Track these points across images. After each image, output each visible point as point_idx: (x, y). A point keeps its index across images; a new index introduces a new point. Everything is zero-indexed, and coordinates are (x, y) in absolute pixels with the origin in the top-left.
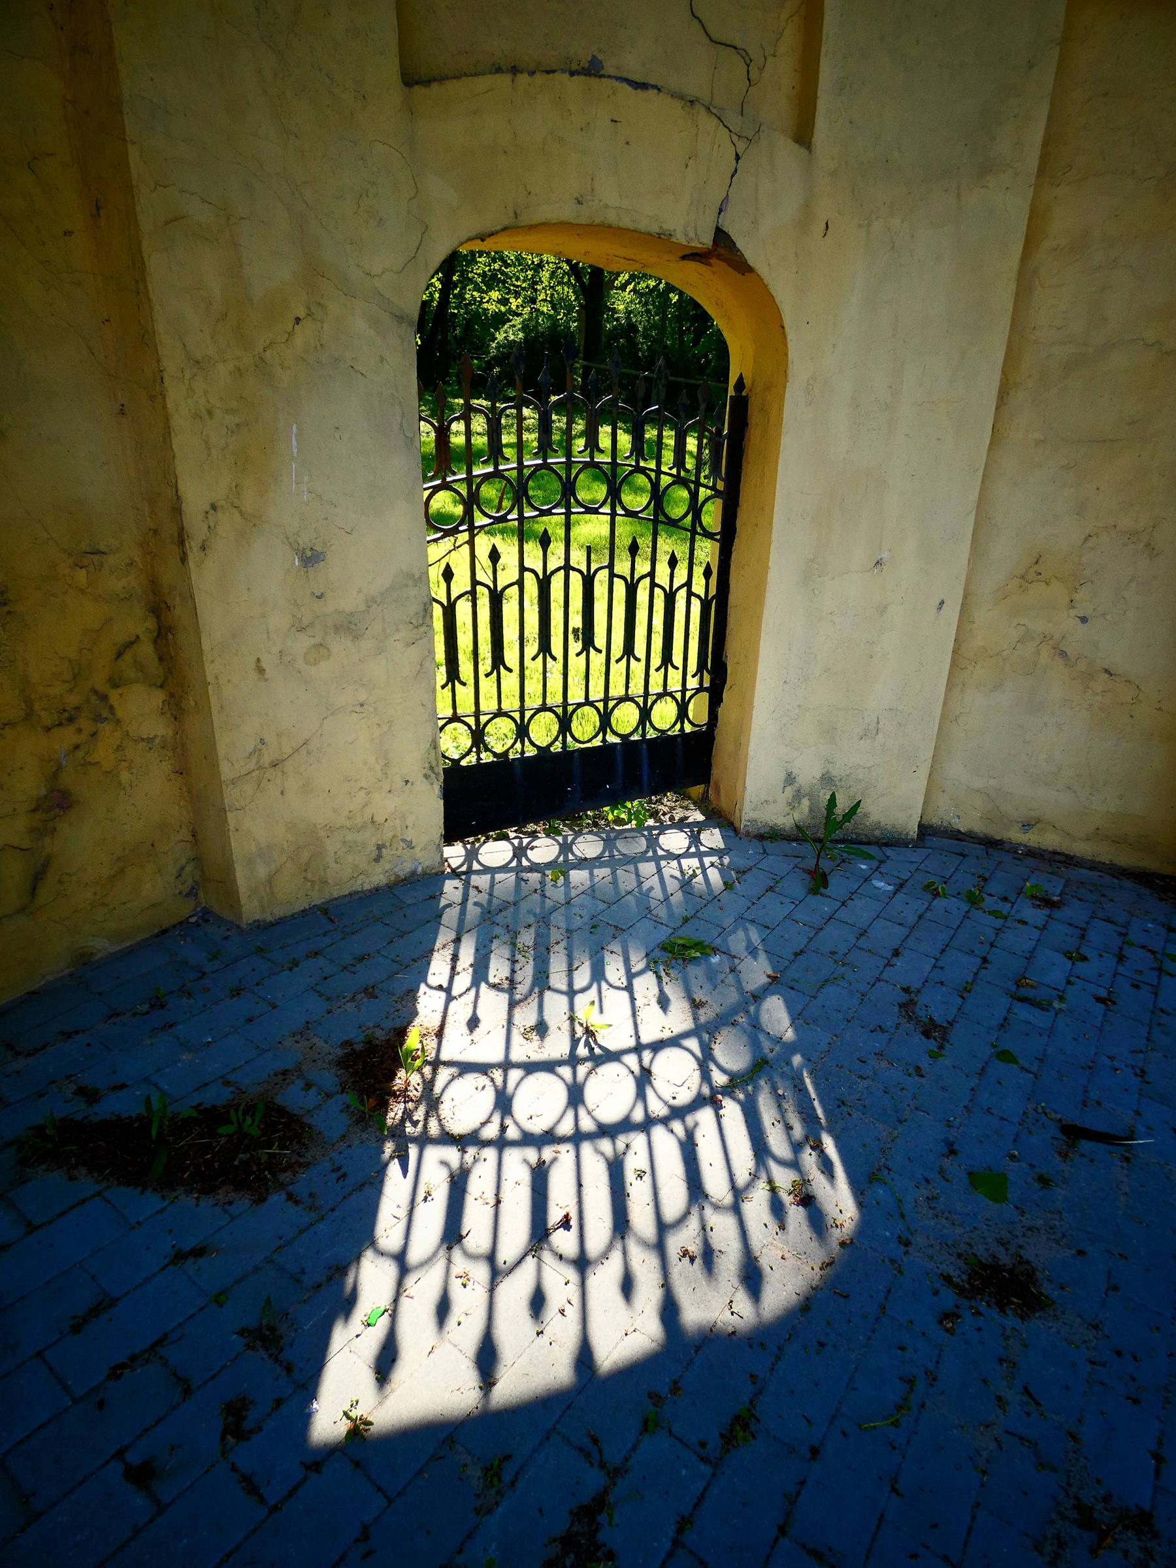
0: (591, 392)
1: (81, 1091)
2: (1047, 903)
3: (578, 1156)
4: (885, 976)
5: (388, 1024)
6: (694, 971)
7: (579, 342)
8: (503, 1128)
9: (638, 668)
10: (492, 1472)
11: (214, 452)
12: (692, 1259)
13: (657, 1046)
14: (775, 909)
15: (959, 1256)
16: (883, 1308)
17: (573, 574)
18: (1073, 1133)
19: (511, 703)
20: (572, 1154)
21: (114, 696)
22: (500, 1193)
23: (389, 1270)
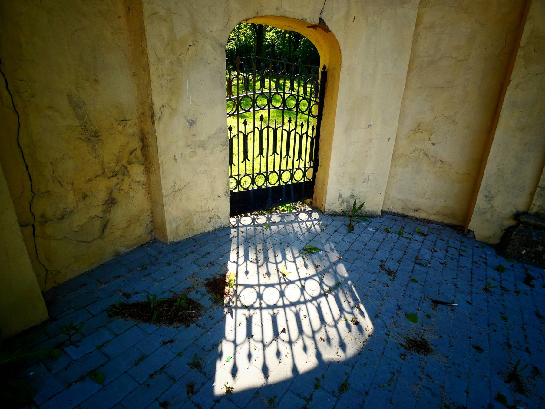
0: (277, 70)
1: (124, 294)
2: (423, 234)
3: (285, 312)
4: (374, 257)
5: (219, 273)
6: (314, 256)
7: (255, 49)
8: (261, 304)
9: (290, 160)
10: (271, 401)
11: (164, 88)
12: (324, 341)
13: (306, 279)
14: (338, 237)
15: (405, 338)
16: (383, 353)
17: (270, 129)
18: (436, 302)
19: (249, 172)
20: (283, 311)
21: (129, 167)
22: (262, 323)
23: (232, 346)
